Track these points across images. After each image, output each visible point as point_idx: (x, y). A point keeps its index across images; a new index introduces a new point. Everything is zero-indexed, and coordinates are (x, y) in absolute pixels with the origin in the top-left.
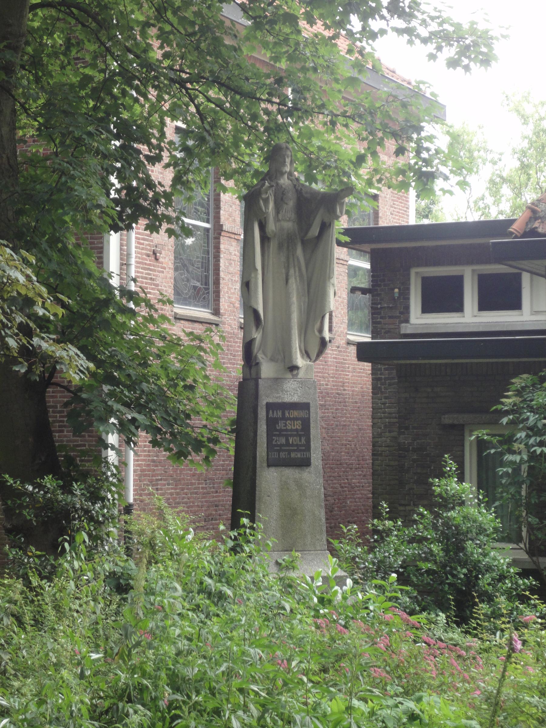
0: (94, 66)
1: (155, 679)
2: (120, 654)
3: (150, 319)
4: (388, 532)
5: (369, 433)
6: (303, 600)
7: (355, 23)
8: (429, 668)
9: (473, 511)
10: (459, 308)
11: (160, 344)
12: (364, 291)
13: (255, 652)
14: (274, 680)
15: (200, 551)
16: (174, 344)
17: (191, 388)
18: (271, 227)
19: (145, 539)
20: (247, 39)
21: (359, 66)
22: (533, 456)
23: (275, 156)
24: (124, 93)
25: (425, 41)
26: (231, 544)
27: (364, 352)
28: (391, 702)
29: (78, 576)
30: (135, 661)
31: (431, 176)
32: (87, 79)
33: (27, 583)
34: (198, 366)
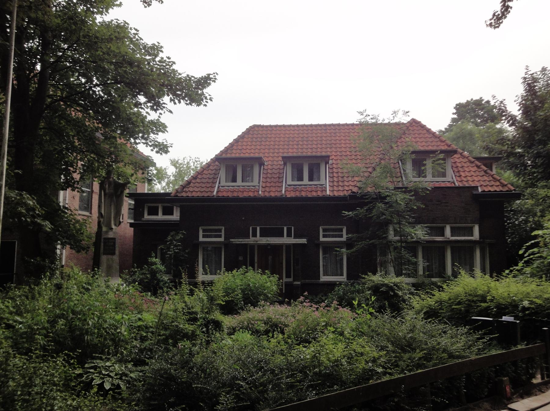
0: (58, 146)
1: (67, 312)
2: (58, 306)
3: (71, 214)
4: (136, 272)
5: (132, 246)
6: (112, 290)
7: (132, 140)
8: (145, 307)
9: (159, 266)
10: (157, 214)
11: (73, 221)
12: (132, 209)
13: (97, 304)
14: (102, 311)
15: (83, 277)
16: (78, 221)
17: (82, 233)
18: (107, 191)
19: (67, 274)
20: (102, 142)
21: (133, 151)
22: (175, 252)
23: (109, 173)
24: (66, 154)
25: (150, 146)
26: (92, 275)
27: (131, 225)
28: (134, 316)
29: (46, 284)
30: (62, 307)
31: (151, 180)
32: (55, 149)
33: (30, 287)
34: (84, 228)
